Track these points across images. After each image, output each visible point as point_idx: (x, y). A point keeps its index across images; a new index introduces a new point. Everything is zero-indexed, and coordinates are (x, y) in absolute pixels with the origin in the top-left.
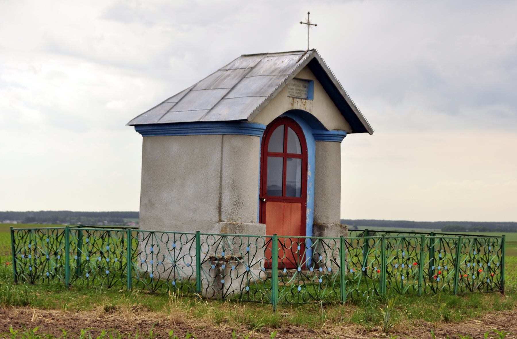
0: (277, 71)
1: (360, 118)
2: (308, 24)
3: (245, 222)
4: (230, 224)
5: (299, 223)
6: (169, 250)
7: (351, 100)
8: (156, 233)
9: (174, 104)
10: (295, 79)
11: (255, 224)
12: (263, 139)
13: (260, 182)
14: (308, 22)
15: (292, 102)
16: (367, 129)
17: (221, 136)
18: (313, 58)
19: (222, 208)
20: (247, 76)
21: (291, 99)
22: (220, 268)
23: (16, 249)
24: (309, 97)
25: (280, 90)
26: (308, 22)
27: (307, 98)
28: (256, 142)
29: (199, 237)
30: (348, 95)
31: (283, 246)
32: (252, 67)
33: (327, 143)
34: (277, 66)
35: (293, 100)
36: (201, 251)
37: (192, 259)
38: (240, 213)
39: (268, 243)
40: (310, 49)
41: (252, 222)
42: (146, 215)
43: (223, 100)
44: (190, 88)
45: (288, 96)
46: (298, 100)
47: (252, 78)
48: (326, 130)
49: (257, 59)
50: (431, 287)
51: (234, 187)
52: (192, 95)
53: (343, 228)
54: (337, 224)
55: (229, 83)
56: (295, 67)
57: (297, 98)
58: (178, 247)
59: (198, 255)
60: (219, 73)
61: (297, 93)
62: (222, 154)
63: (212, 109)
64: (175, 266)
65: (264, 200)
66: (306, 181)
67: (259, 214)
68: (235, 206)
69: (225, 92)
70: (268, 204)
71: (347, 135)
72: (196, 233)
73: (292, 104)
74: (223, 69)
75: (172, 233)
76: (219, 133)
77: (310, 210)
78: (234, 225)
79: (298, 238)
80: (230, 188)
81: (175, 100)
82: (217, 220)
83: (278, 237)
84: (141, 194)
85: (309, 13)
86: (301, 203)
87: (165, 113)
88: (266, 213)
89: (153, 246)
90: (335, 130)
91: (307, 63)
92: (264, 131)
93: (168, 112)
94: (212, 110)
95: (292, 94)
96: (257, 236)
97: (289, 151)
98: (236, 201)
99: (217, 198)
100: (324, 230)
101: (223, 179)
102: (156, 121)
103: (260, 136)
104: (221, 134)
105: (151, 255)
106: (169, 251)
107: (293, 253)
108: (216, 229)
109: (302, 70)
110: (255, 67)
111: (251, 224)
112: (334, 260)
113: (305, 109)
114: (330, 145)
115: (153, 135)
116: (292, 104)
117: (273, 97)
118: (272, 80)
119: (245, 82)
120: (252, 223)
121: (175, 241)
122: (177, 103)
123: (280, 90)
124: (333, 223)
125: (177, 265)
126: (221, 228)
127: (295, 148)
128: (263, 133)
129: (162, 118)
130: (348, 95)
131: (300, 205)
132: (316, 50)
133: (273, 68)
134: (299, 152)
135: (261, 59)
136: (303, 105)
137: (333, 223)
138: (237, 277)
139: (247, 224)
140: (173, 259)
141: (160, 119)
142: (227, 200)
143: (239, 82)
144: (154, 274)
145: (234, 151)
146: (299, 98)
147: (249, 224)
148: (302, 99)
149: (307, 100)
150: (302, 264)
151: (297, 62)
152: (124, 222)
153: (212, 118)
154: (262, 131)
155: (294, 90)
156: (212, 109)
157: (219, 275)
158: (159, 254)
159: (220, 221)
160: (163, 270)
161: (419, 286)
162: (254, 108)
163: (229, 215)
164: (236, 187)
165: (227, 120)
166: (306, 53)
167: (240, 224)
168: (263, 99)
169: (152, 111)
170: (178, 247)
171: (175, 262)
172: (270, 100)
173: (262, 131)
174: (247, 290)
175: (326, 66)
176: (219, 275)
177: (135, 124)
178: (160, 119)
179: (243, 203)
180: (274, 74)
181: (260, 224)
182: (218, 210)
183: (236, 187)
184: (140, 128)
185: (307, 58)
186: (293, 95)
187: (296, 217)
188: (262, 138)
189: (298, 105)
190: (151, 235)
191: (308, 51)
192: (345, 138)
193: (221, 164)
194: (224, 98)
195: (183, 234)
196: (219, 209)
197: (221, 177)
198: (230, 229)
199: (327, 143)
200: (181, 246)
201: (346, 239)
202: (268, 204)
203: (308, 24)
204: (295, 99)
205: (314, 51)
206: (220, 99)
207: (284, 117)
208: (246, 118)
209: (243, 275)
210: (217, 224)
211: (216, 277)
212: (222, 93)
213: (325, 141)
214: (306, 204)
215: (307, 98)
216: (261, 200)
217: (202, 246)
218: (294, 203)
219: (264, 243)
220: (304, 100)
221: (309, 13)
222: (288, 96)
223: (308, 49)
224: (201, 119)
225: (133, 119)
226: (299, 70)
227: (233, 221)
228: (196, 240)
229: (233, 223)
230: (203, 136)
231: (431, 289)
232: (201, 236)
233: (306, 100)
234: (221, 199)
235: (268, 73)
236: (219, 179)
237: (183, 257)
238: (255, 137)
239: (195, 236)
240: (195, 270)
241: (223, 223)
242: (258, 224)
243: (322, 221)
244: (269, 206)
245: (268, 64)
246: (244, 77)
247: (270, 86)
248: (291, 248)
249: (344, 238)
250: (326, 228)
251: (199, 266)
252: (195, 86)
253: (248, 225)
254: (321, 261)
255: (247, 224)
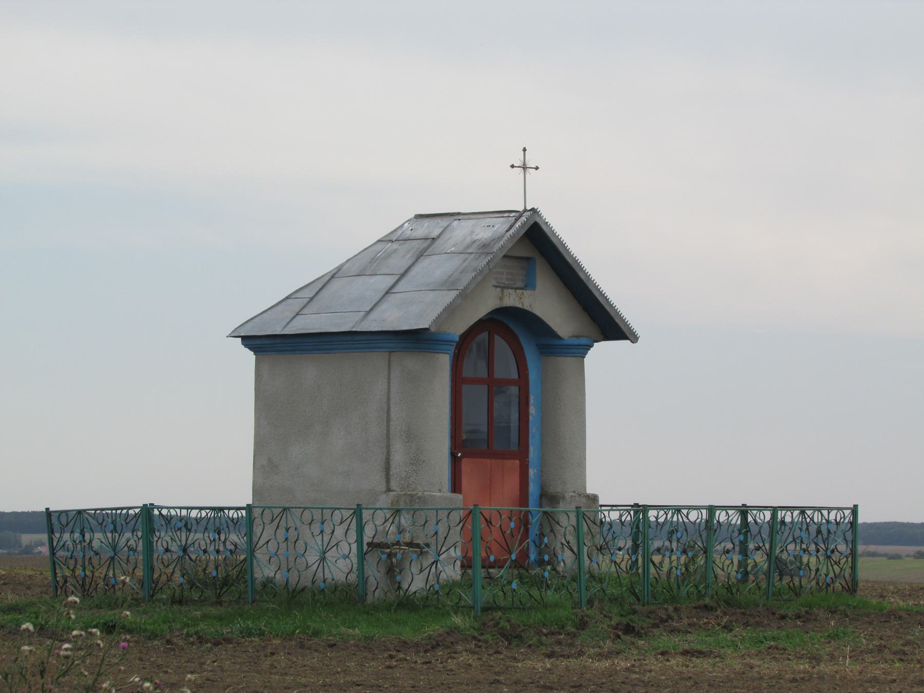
0: (475, 246)
1: (614, 317)
2: (524, 167)
3: (429, 491)
4: (404, 494)
5: (517, 492)
6: (314, 534)
7: (599, 287)
8: (292, 510)
9: (306, 301)
10: (505, 256)
11: (444, 494)
12: (454, 356)
13: (450, 426)
14: (524, 164)
15: (501, 296)
16: (628, 335)
17: (388, 353)
18: (533, 222)
19: (391, 469)
20: (425, 254)
21: (499, 289)
22: (394, 560)
23: (55, 544)
24: (529, 285)
25: (481, 279)
26: (524, 164)
27: (526, 286)
28: (444, 361)
29: (361, 514)
30: (592, 280)
31: (489, 522)
32: (433, 237)
33: (561, 359)
34: (475, 237)
35: (502, 292)
36: (364, 535)
37: (350, 546)
38: (421, 477)
39: (466, 518)
40: (528, 208)
41: (440, 491)
42: (264, 483)
43: (388, 295)
44: (332, 274)
45: (493, 286)
46: (510, 291)
47: (434, 257)
48: (559, 338)
49: (444, 222)
50: (727, 588)
51: (410, 436)
52: (336, 285)
53: (591, 499)
54: (579, 493)
55: (399, 263)
56: (504, 240)
57: (508, 288)
58: (328, 531)
59: (360, 540)
60: (379, 247)
61: (508, 279)
62: (389, 383)
63: (371, 310)
64: (324, 558)
65: (459, 455)
66: (527, 422)
67: (450, 423)
68: (412, 467)
69: (390, 280)
70: (464, 461)
71: (595, 344)
72: (356, 507)
73: (501, 299)
74: (385, 239)
75: (318, 508)
76: (384, 350)
77: (535, 471)
78: (412, 496)
79: (511, 511)
80: (403, 437)
81: (309, 293)
82: (384, 489)
83: (480, 509)
84: (254, 451)
85: (525, 150)
86: (520, 460)
87: (293, 316)
88: (463, 478)
89: (287, 530)
90: (573, 336)
91: (523, 232)
92: (455, 344)
93: (298, 314)
94: (371, 312)
95: (500, 281)
96: (450, 509)
97: (498, 375)
98: (414, 458)
99: (383, 453)
100: (559, 504)
101: (392, 423)
102: (278, 331)
103: (449, 352)
104: (386, 352)
105: (325, 518)
106: (313, 536)
107: (503, 533)
108: (384, 501)
109: (515, 244)
110: (439, 237)
111: (439, 494)
112: (567, 544)
113: (523, 305)
114: (567, 362)
115: (273, 353)
116: (500, 298)
117: (469, 291)
118: (467, 261)
119: (424, 263)
120: (440, 492)
121: (324, 519)
122: (312, 299)
123: (480, 278)
124: (574, 492)
125: (328, 558)
126: (390, 502)
127: (506, 367)
128: (454, 347)
129: (289, 326)
130: (592, 280)
131: (518, 462)
132: (538, 210)
133: (468, 240)
134: (514, 375)
135: (449, 223)
136: (518, 299)
137: (574, 492)
138: (421, 571)
139: (433, 494)
140: (321, 547)
141: (285, 327)
142: (399, 457)
143: (413, 264)
144: (290, 572)
145: (409, 377)
146: (512, 288)
147: (435, 494)
148: (516, 289)
149: (526, 290)
150: (517, 549)
151: (507, 231)
152: (20, 546)
153: (373, 325)
154: (453, 345)
155: (503, 275)
156: (371, 310)
157: (392, 571)
158: (297, 542)
159: (389, 490)
160: (306, 566)
161: (707, 585)
162: (438, 310)
163: (402, 480)
164: (412, 436)
165: (397, 329)
166: (520, 214)
167: (420, 494)
168: (453, 294)
169: (269, 312)
170: (328, 531)
171: (324, 553)
172: (465, 296)
173: (453, 345)
174: (436, 590)
175: (554, 234)
176: (392, 571)
177: (242, 335)
178: (285, 327)
179: (424, 461)
180: (470, 251)
181: (452, 494)
182: (385, 473)
183: (412, 436)
184: (249, 341)
185: (523, 225)
186: (503, 283)
187: (512, 484)
188: (452, 355)
189: (511, 298)
190: (284, 516)
191: (525, 210)
192: (591, 349)
193: (389, 399)
194: (390, 292)
195: (336, 509)
196: (386, 472)
197: (388, 420)
198: (405, 502)
199: (564, 359)
200: (333, 528)
201: (584, 511)
202: (464, 461)
203: (524, 168)
204: (505, 290)
205: (534, 211)
206: (383, 293)
207: (488, 318)
208: (426, 326)
209: (429, 568)
210: (384, 495)
211: (388, 573)
212: (384, 282)
213: (557, 356)
214: (528, 461)
215: (524, 288)
216: (453, 455)
217: (366, 526)
218: (508, 459)
219: (460, 519)
220: (521, 291)
221: (525, 150)
222: (493, 286)
223: (525, 208)
224: (354, 327)
225: (239, 327)
226: (511, 245)
227: (409, 491)
228: (356, 518)
229: (409, 493)
230: (357, 354)
231: (728, 591)
232: (363, 511)
233: (524, 291)
234: (389, 455)
235: (460, 249)
236: (386, 422)
237: (337, 545)
238: (441, 354)
239: (354, 512)
240: (355, 566)
241: (393, 493)
242: (450, 494)
243: (553, 489)
244: (467, 465)
245: (461, 232)
246: (422, 255)
247: (464, 271)
248: (501, 525)
249: (583, 510)
250: (561, 501)
251: (362, 556)
252: (339, 269)
253: (434, 495)
254: (546, 545)
255: (433, 494)
